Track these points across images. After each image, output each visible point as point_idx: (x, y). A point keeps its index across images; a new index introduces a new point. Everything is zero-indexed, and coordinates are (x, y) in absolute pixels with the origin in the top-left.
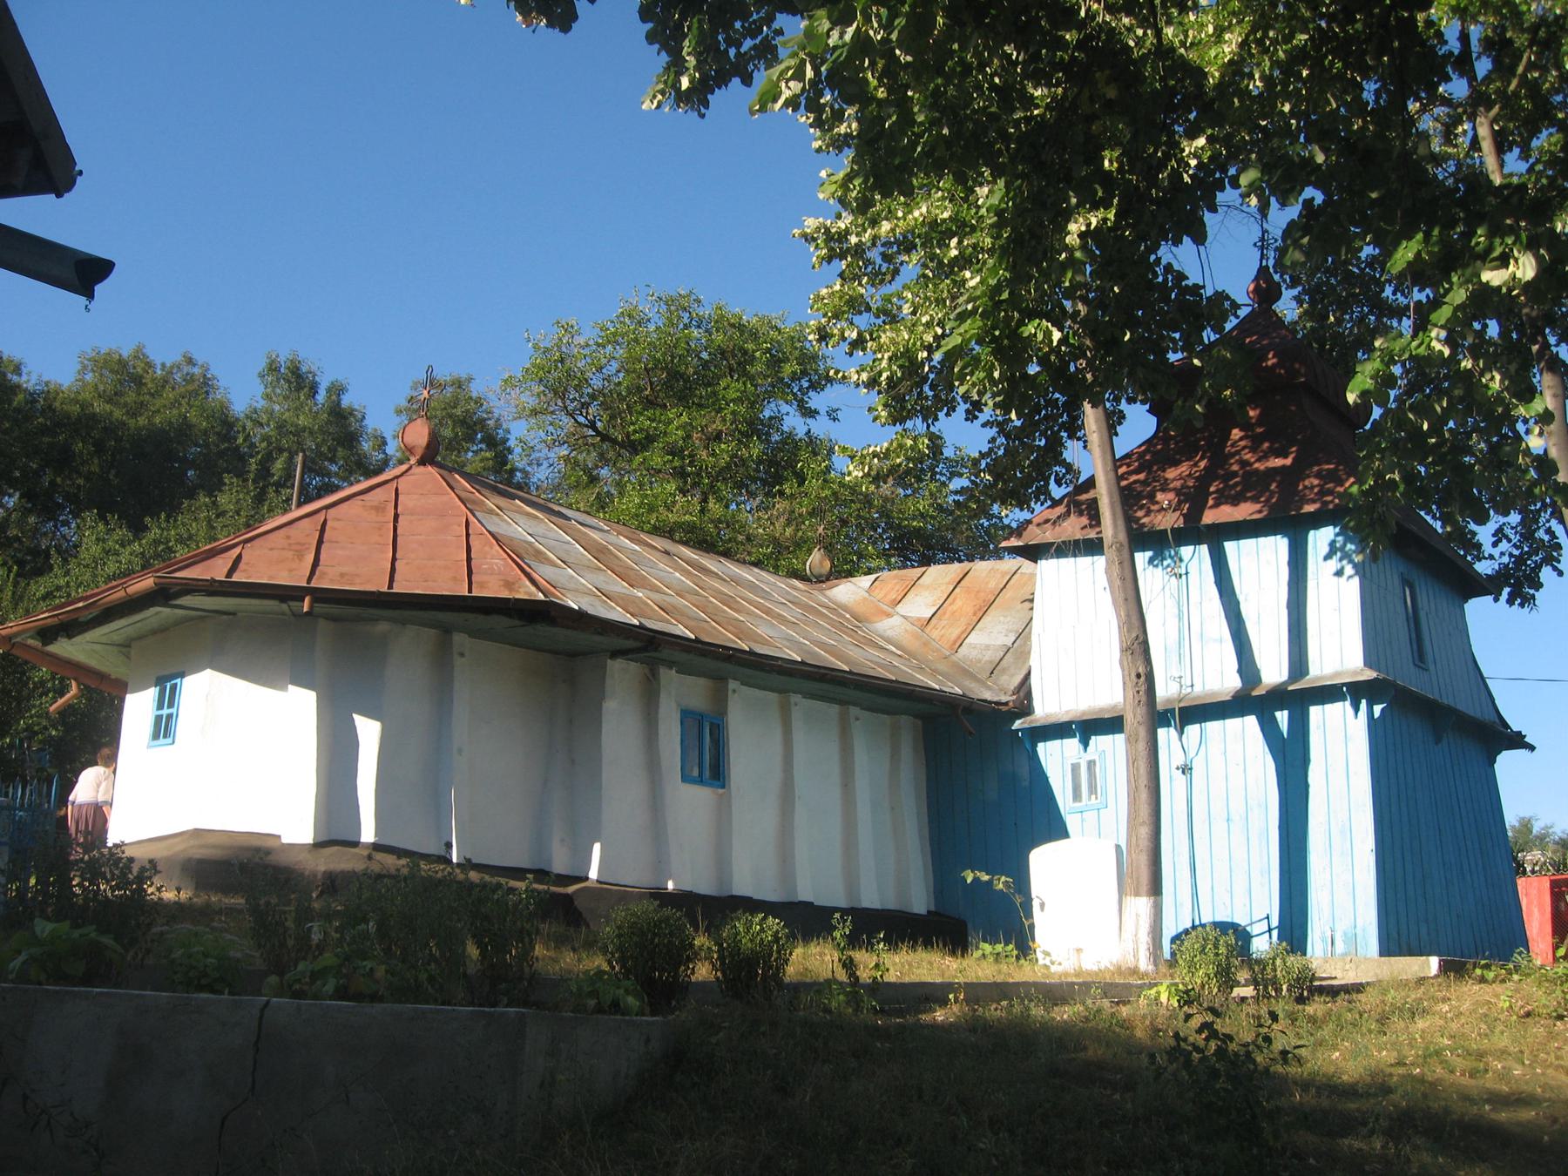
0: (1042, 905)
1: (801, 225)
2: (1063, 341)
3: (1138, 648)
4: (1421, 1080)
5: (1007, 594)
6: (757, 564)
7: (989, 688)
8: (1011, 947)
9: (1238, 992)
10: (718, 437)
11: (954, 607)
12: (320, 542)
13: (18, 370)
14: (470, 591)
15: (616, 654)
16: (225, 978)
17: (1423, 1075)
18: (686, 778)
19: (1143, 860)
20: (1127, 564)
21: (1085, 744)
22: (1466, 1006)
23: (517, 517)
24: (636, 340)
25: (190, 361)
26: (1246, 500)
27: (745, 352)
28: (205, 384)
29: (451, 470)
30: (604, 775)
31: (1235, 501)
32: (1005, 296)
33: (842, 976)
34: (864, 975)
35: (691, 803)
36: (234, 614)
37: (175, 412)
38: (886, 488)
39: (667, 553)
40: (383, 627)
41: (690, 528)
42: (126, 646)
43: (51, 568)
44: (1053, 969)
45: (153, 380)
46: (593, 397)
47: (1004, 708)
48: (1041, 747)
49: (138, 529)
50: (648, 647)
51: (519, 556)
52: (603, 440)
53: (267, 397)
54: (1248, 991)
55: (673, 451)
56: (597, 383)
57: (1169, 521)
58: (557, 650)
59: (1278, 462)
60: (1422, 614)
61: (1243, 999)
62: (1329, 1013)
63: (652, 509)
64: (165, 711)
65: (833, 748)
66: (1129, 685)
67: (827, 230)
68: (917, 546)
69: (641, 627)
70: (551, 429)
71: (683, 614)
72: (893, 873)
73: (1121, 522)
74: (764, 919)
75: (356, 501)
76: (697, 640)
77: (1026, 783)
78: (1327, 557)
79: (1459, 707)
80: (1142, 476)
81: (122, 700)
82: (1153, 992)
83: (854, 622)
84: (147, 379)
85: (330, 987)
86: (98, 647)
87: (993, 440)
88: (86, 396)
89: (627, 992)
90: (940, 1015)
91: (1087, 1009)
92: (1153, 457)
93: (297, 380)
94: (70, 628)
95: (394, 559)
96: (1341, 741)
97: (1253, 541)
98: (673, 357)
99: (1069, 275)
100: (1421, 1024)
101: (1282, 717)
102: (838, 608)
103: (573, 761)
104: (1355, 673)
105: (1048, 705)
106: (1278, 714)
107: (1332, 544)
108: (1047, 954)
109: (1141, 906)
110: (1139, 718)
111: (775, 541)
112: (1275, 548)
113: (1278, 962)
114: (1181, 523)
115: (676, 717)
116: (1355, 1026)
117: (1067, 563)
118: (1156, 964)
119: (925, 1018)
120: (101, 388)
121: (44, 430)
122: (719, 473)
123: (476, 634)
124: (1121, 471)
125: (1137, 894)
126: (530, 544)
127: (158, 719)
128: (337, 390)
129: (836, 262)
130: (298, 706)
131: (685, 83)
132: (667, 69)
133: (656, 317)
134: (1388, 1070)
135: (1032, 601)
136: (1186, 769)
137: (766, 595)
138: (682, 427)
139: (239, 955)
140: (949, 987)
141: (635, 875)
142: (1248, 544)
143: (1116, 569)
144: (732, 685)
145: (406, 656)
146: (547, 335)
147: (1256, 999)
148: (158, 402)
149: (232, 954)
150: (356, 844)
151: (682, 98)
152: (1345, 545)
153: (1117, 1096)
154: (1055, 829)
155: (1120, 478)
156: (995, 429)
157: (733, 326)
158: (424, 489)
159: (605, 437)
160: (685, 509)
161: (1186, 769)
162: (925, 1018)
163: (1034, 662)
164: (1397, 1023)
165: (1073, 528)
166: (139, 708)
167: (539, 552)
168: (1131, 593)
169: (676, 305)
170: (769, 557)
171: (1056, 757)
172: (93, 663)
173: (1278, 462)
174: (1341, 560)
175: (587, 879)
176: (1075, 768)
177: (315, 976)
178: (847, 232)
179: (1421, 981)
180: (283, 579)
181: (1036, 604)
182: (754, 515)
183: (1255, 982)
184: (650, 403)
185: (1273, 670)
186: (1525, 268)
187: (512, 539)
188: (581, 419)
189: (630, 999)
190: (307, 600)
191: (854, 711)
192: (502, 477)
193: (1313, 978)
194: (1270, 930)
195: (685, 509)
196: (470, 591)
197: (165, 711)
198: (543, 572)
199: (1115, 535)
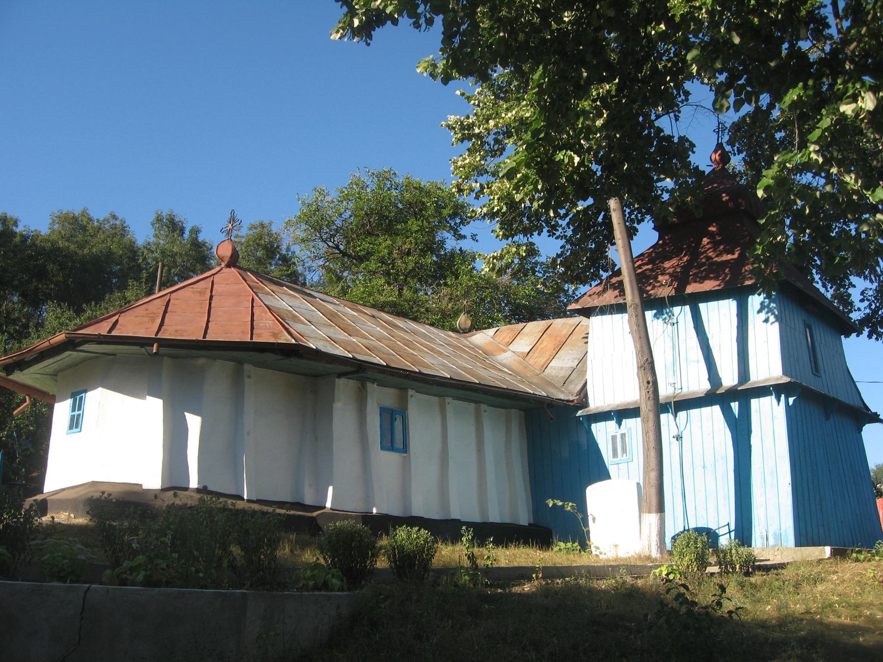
0: (594, 519)
1: (446, 120)
2: (581, 163)
3: (647, 365)
4: (821, 623)
5: (573, 337)
6: (432, 325)
7: (562, 392)
8: (576, 544)
9: (710, 569)
10: (409, 254)
11: (542, 346)
12: (165, 312)
13: (16, 223)
14: (251, 338)
15: (340, 375)
16: (75, 573)
17: (821, 619)
18: (382, 448)
19: (653, 492)
20: (640, 316)
21: (620, 424)
22: (847, 576)
23: (283, 296)
24: (360, 198)
25: (115, 217)
26: (711, 279)
27: (423, 203)
28: (122, 231)
29: (245, 270)
30: (334, 447)
31: (702, 280)
32: (542, 135)
33: (466, 563)
34: (480, 563)
35: (386, 462)
36: (115, 355)
37: (104, 245)
38: (505, 278)
39: (373, 317)
40: (202, 361)
41: (394, 305)
42: (54, 375)
43: (29, 334)
44: (601, 557)
45: (92, 228)
46: (337, 231)
47: (571, 404)
48: (593, 426)
49: (79, 311)
50: (358, 370)
51: (282, 319)
52: (343, 256)
53: (156, 236)
54: (715, 569)
55: (383, 262)
56: (339, 223)
57: (665, 292)
58: (305, 372)
59: (730, 257)
60: (817, 344)
61: (712, 574)
62: (764, 582)
63: (370, 295)
64: (76, 413)
65: (472, 429)
66: (643, 388)
67: (462, 123)
68: (523, 313)
69: (354, 358)
70: (313, 250)
71: (379, 351)
72: (508, 503)
73: (636, 292)
74: (419, 530)
75: (189, 289)
76: (387, 366)
77: (586, 447)
78: (759, 312)
79: (840, 398)
80: (650, 266)
81: (51, 408)
82: (657, 571)
83: (484, 355)
84: (89, 227)
85: (141, 577)
86: (38, 376)
87: (563, 247)
88: (54, 237)
89: (333, 576)
90: (527, 588)
91: (617, 582)
92: (656, 255)
93: (173, 226)
94: (21, 365)
95: (208, 321)
96: (770, 419)
97: (716, 302)
98: (382, 207)
99: (581, 120)
100: (820, 588)
101: (735, 406)
102: (475, 347)
103: (316, 439)
104: (777, 379)
105: (597, 402)
106: (732, 404)
107: (762, 303)
108: (597, 548)
109: (652, 519)
110: (649, 408)
111: (443, 312)
112: (729, 306)
113: (733, 551)
114: (673, 293)
115: (377, 412)
116: (780, 589)
117: (607, 318)
118: (661, 553)
119: (517, 589)
120: (63, 233)
121: (31, 257)
122: (409, 273)
123: (258, 364)
124: (638, 264)
125: (650, 512)
126: (290, 311)
127: (73, 417)
128: (196, 231)
129: (466, 142)
130: (152, 409)
131: (356, 22)
132: (346, 15)
133: (372, 185)
134: (802, 616)
135: (587, 338)
136: (679, 438)
137: (432, 340)
138: (388, 247)
139: (84, 558)
140: (533, 569)
141: (354, 505)
142: (713, 305)
143: (634, 320)
144: (411, 392)
145: (216, 378)
146: (309, 196)
147: (720, 574)
148: (95, 240)
149: (79, 557)
150: (186, 489)
151: (356, 32)
152: (769, 304)
153: (632, 637)
154: (603, 474)
155: (635, 269)
156: (564, 240)
157: (415, 188)
158: (228, 280)
159: (344, 254)
160: (390, 294)
161: (679, 438)
162: (517, 589)
163: (589, 376)
164: (806, 587)
165: (610, 297)
166: (62, 411)
167: (295, 316)
168: (643, 334)
169: (383, 178)
170: (439, 321)
171: (602, 432)
172: (38, 386)
173: (730, 257)
174: (767, 313)
175: (325, 507)
176: (614, 438)
177: (132, 570)
178: (473, 124)
179: (820, 561)
180: (142, 333)
181: (590, 339)
182: (432, 297)
183: (719, 563)
184: (370, 234)
185: (729, 378)
186: (868, 102)
187: (279, 309)
188: (331, 244)
189: (335, 581)
190: (155, 345)
191: (483, 407)
192: (294, 280)
193: (755, 560)
194: (730, 532)
195: (390, 294)
196: (251, 338)
197: (76, 413)
198: (296, 328)
199: (633, 300)
